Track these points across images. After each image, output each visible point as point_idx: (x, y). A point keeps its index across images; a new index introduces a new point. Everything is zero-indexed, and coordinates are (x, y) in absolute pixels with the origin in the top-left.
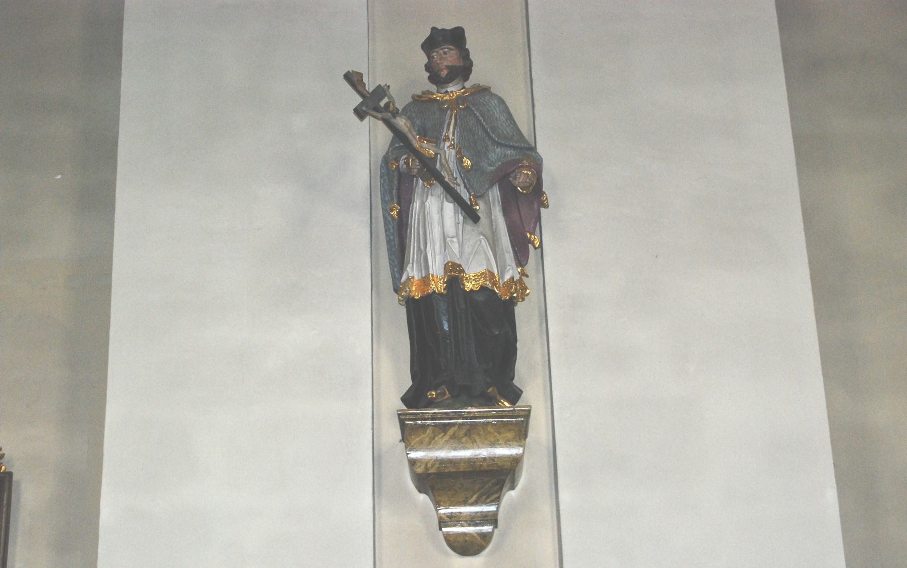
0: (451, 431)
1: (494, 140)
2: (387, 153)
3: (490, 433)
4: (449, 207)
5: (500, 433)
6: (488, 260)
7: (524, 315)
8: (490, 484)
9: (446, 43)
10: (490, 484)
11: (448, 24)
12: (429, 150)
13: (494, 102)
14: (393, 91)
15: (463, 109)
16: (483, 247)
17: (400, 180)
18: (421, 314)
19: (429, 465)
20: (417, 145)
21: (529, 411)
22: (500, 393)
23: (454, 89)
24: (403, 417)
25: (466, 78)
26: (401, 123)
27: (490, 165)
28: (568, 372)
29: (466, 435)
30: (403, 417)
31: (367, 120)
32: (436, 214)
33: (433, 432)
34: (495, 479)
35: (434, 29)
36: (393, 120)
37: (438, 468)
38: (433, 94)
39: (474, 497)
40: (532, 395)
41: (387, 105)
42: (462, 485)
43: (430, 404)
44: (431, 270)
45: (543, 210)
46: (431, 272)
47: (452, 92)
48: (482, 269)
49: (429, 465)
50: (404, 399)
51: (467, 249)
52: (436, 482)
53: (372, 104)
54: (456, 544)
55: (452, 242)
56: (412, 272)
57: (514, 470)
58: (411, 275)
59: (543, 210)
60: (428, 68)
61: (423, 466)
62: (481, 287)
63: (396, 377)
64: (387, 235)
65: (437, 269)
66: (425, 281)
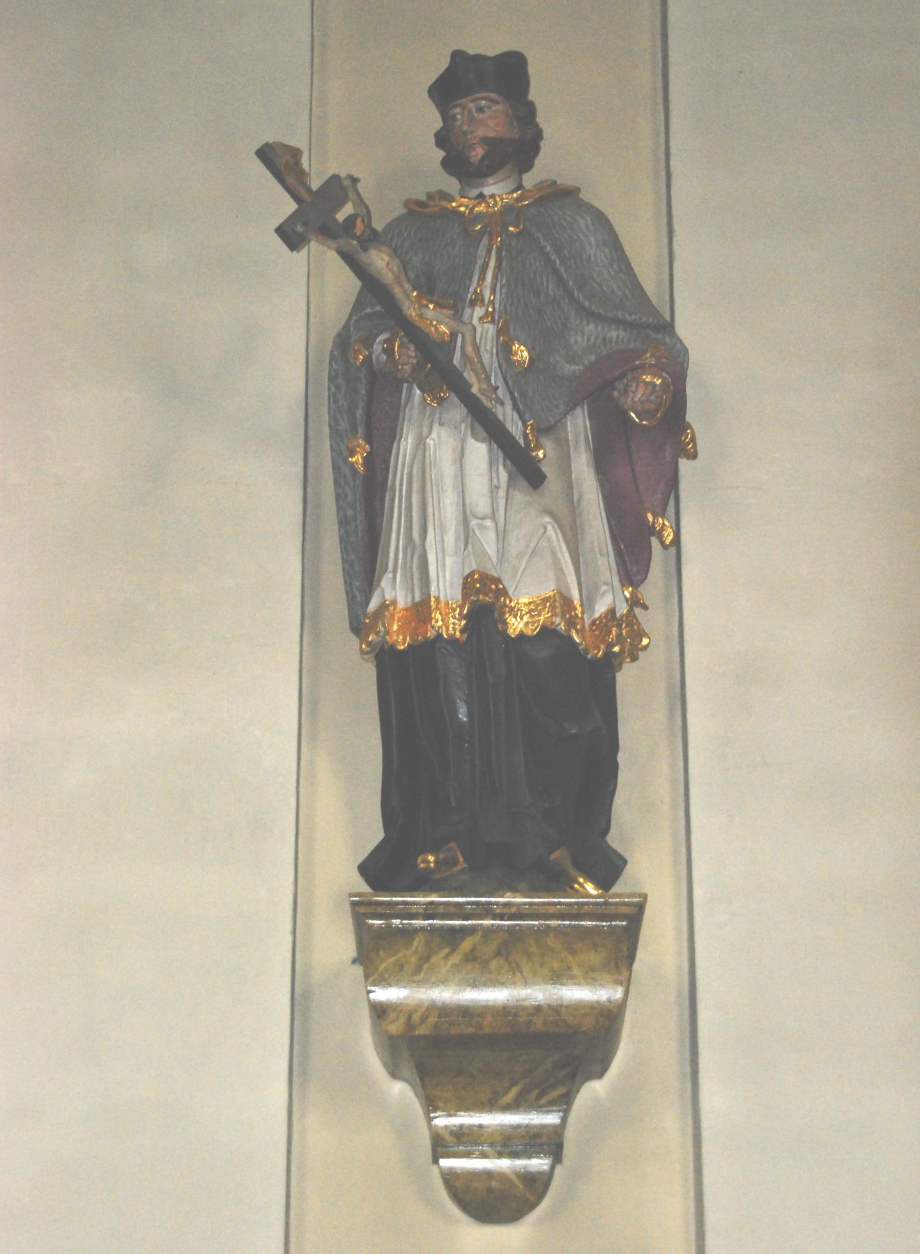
6: (559, 570)
9: (486, 95)
12: (438, 323)
13: (584, 222)
19: (416, 1018)
21: (641, 907)
23: (498, 191)
27: (571, 361)
29: (498, 953)
30: (362, 910)
34: (562, 1054)
36: (363, 257)
40: (648, 871)
43: (423, 882)
44: (433, 588)
45: (684, 464)
47: (493, 196)
48: (548, 590)
49: (416, 1018)
50: (366, 869)
51: (516, 543)
53: (317, 215)
55: (480, 528)
56: (394, 591)
58: (389, 596)
59: (684, 464)
60: (441, 139)
61: (402, 1021)
63: (348, 822)
65: (446, 585)
66: (421, 611)
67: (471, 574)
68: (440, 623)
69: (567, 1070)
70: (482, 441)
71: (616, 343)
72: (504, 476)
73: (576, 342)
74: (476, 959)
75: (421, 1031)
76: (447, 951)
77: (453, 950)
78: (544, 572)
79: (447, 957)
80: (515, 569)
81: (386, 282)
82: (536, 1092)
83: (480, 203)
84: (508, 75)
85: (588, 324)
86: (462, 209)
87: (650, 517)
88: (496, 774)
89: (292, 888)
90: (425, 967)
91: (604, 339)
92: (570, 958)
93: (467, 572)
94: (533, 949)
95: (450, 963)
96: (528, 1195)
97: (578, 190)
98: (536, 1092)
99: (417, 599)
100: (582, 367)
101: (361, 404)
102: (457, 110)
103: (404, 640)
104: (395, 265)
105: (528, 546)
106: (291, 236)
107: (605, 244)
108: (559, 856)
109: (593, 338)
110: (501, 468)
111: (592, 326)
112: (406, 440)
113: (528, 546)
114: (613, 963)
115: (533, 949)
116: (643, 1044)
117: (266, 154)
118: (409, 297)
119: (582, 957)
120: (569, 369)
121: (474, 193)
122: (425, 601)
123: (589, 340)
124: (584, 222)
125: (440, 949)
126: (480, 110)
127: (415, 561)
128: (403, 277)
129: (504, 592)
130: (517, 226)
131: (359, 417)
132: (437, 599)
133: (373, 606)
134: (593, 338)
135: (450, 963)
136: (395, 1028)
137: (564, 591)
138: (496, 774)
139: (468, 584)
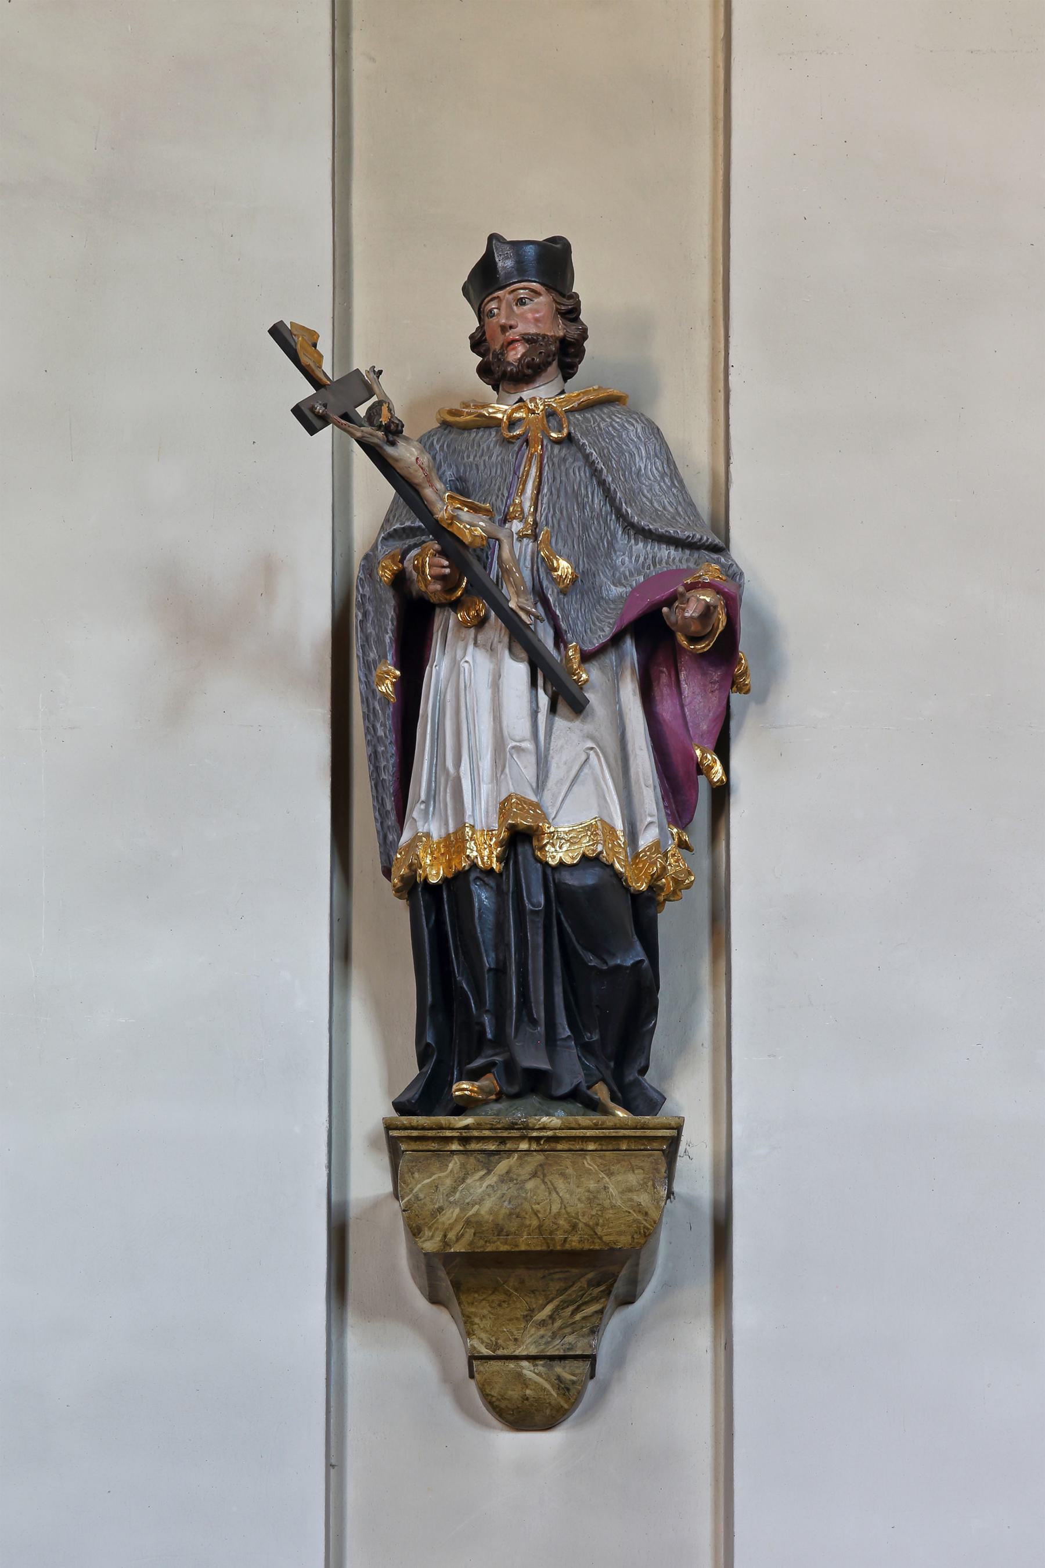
0: (503, 1166)
1: (632, 525)
2: (375, 548)
3: (589, 1172)
4: (516, 672)
5: (610, 1174)
6: (602, 797)
7: (677, 925)
8: (583, 1282)
9: (526, 285)
10: (583, 1282)
11: (531, 229)
12: (472, 527)
13: (635, 431)
14: (389, 386)
15: (558, 442)
16: (592, 768)
17: (404, 612)
18: (439, 910)
19: (451, 1235)
20: (442, 511)
21: (679, 1128)
22: (614, 1099)
23: (542, 393)
24: (394, 1133)
25: (568, 371)
26: (407, 453)
27: (617, 583)
28: (781, 1068)
29: (534, 1175)
30: (394, 1133)
31: (326, 432)
32: (478, 683)
33: (463, 1166)
34: (599, 1272)
35: (493, 238)
36: (390, 450)
37: (471, 1243)
38: (485, 406)
39: (548, 1309)
40: (687, 1097)
41: (374, 412)
42: (522, 1282)
43: (461, 1108)
44: (468, 812)
45: (735, 698)
46: (469, 821)
47: (533, 399)
48: (588, 817)
49: (451, 1235)
50: (400, 1107)
51: (558, 771)
52: (466, 1273)
53: (335, 403)
54: (503, 1404)
55: (521, 757)
56: (426, 824)
57: (638, 1253)
58: (422, 828)
59: (735, 698)
60: (478, 343)
61: (438, 1238)
62: (584, 857)
63: (378, 1073)
64: (369, 743)
65: (482, 813)
66: (455, 842)
67: (508, 798)
68: (475, 854)
69: (602, 1288)
70: (521, 660)
71: (667, 563)
72: (544, 700)
73: (623, 563)
74: (511, 1180)
75: (458, 1248)
76: (482, 1173)
77: (489, 1172)
78: (589, 797)
79: (482, 1178)
80: (555, 796)
81: (416, 481)
82: (571, 1308)
83: (520, 408)
84: (552, 262)
85: (637, 544)
86: (499, 416)
87: (698, 752)
88: (536, 1005)
89: (327, 1124)
90: (460, 1188)
91: (654, 558)
92: (607, 1179)
93: (503, 796)
94: (570, 1171)
95: (485, 1185)
96: (562, 1403)
97: (627, 397)
98: (571, 1308)
99: (451, 830)
100: (629, 589)
101: (390, 627)
102: (493, 305)
103: (438, 873)
104: (425, 459)
105: (568, 772)
106: (309, 418)
107: (656, 455)
108: (601, 1092)
109: (642, 559)
110: (541, 691)
111: (641, 545)
112: (439, 665)
113: (568, 772)
114: (650, 1184)
115: (570, 1171)
116: (678, 1250)
117: (278, 332)
118: (442, 500)
119: (620, 1178)
120: (616, 591)
121: (516, 397)
122: (461, 826)
123: (637, 561)
124: (635, 431)
125: (476, 1170)
126: (521, 302)
127: (448, 795)
128: (434, 475)
129: (545, 817)
130: (560, 431)
131: (388, 640)
132: (472, 827)
133: (406, 836)
134: (642, 559)
135: (485, 1185)
136: (430, 1245)
137: (607, 820)
138: (536, 1005)
139: (504, 807)
